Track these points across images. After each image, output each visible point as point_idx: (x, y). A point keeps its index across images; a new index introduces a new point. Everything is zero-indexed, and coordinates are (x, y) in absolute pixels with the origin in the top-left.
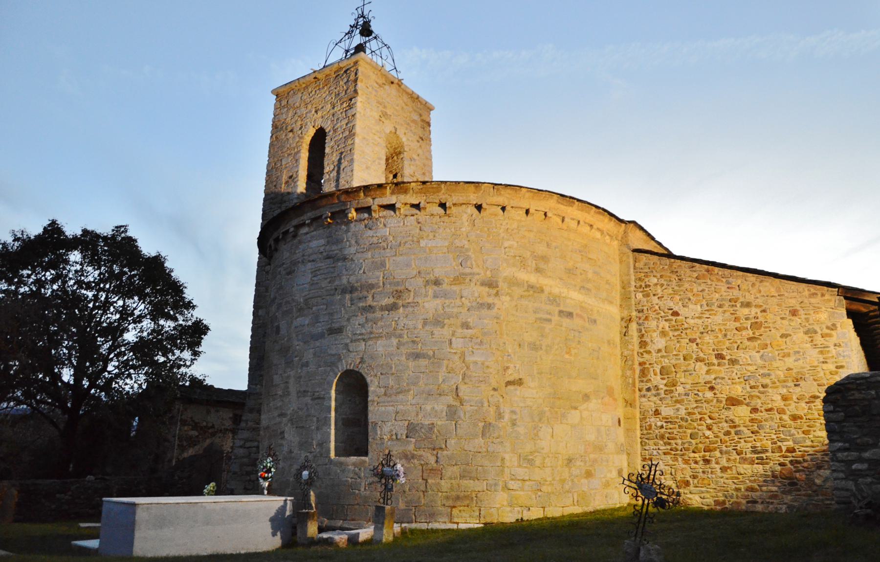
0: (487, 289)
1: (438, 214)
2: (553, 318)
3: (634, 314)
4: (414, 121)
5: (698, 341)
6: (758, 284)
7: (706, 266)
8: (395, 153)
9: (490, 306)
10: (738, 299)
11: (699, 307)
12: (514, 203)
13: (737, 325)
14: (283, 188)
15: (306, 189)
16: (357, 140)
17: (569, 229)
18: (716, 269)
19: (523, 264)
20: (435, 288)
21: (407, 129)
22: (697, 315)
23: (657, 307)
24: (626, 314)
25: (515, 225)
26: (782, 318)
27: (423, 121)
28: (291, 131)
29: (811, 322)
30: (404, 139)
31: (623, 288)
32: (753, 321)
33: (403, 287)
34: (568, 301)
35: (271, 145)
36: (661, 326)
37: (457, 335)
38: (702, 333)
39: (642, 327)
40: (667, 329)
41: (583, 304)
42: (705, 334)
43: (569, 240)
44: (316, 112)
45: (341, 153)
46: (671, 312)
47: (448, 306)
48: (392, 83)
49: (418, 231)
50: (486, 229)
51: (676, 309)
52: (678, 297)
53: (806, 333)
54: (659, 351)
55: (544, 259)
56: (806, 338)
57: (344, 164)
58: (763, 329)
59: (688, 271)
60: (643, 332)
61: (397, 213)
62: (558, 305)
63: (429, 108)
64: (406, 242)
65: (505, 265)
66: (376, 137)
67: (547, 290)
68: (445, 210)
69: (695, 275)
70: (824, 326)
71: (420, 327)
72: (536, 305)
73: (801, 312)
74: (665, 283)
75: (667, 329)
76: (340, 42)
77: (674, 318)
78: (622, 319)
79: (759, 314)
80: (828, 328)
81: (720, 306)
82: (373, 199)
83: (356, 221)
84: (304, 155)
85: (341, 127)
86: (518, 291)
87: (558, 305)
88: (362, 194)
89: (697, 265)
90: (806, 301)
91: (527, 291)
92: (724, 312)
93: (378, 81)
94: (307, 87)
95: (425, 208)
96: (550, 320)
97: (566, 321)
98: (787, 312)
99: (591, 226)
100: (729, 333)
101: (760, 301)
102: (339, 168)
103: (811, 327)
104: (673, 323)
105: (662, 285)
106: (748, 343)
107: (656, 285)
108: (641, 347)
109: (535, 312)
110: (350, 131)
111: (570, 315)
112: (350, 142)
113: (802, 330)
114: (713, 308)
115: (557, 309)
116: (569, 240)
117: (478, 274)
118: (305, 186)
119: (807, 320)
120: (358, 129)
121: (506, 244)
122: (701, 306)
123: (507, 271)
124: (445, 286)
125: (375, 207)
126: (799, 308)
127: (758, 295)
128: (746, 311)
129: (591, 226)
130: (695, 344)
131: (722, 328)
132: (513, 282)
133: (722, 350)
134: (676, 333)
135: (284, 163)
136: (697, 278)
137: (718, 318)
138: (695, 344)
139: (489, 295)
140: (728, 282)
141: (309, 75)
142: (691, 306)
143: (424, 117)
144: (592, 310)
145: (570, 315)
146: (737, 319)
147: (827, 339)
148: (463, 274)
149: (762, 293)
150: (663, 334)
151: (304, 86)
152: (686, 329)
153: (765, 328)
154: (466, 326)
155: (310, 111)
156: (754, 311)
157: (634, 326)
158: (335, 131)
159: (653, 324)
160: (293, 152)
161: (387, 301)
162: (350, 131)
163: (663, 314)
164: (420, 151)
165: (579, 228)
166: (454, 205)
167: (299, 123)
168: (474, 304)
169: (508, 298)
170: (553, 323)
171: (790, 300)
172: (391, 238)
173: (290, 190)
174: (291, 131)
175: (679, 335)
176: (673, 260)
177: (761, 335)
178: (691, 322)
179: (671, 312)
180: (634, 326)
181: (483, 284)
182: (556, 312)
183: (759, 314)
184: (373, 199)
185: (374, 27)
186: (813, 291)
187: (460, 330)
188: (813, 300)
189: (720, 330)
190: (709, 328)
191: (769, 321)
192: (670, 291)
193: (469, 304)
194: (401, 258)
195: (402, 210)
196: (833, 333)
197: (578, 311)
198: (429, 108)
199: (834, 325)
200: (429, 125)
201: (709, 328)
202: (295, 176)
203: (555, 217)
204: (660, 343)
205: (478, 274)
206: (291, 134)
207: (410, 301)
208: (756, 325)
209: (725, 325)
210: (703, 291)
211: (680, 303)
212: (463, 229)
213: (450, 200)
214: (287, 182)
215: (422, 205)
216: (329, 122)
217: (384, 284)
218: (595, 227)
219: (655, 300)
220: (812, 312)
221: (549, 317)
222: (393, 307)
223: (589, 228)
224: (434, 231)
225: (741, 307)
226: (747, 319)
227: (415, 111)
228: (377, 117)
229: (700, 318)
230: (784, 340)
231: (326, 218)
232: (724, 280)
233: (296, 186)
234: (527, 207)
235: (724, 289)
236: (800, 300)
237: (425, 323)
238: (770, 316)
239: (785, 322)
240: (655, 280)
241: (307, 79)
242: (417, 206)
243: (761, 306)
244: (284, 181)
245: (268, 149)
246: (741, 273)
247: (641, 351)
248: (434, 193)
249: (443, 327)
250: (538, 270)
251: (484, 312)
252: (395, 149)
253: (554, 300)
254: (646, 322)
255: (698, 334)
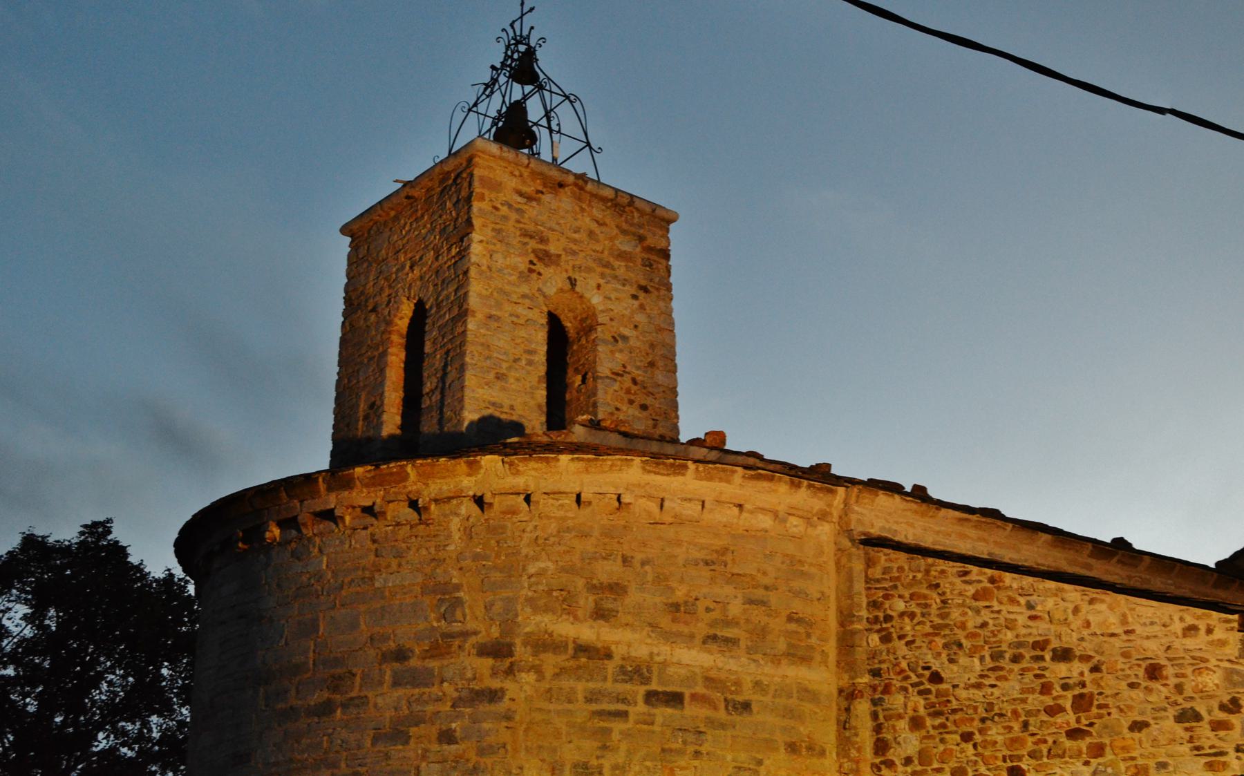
0: (490, 661)
1: (408, 523)
2: (631, 709)
3: (865, 679)
4: (622, 255)
5: (978, 738)
6: (1085, 607)
7: (989, 572)
8: (584, 329)
9: (494, 696)
10: (1047, 642)
11: (976, 661)
12: (549, 484)
13: (1048, 700)
14: (361, 428)
15: (402, 427)
16: (471, 325)
17: (679, 521)
18: (1008, 577)
19: (567, 605)
20: (396, 665)
21: (603, 275)
22: (973, 681)
23: (904, 665)
24: (845, 681)
25: (553, 527)
26: (1132, 686)
27: (649, 249)
28: (374, 310)
29: (1188, 692)
30: (596, 300)
31: (842, 624)
32: (1077, 691)
33: (345, 670)
34: (671, 670)
35: (343, 342)
36: (911, 705)
37: (432, 757)
38: (983, 720)
39: (879, 709)
40: (922, 711)
41: (713, 674)
42: (989, 723)
43: (679, 543)
44: (411, 267)
45: (447, 353)
46: (927, 673)
47: (418, 700)
48: (561, 185)
49: (372, 557)
50: (493, 543)
51: (936, 666)
52: (940, 641)
53: (1180, 718)
54: (908, 761)
55: (617, 589)
56: (1179, 729)
57: (452, 374)
58: (1094, 710)
59: (958, 581)
60: (881, 719)
61: (341, 525)
62: (646, 681)
63: (661, 219)
64: (353, 580)
65: (528, 610)
66: (520, 310)
67: (618, 651)
68: (419, 514)
69: (971, 590)
70: (1216, 706)
71: (368, 743)
72: (591, 685)
73: (1169, 671)
74: (918, 611)
75: (922, 711)
76: (476, 105)
77: (933, 688)
78: (841, 691)
79: (1088, 677)
80: (1223, 707)
81: (1016, 659)
82: (301, 502)
83: (279, 544)
84: (396, 358)
85: (448, 297)
86: (551, 661)
87: (646, 681)
88: (284, 495)
89: (975, 569)
90: (1177, 644)
91: (575, 657)
92: (1023, 671)
93: (525, 189)
94: (396, 218)
95: (383, 514)
96: (623, 715)
97: (663, 713)
98: (1141, 672)
99: (740, 506)
100: (1032, 720)
101: (1088, 647)
102: (444, 383)
103: (1188, 705)
104: (932, 698)
105: (912, 616)
106: (1068, 743)
107: (902, 615)
108: (876, 753)
109: (589, 700)
110: (460, 307)
111: (675, 699)
112: (459, 329)
113: (1172, 712)
114: (1002, 663)
115: (642, 690)
116: (679, 543)
117: (475, 633)
118: (398, 420)
119: (1179, 688)
120: (473, 301)
121: (532, 569)
122: (982, 659)
123: (532, 622)
124: (414, 662)
125: (304, 517)
126: (1163, 662)
127: (1085, 632)
128: (1062, 669)
129: (740, 506)
130: (970, 746)
131: (1019, 708)
132: (544, 644)
133: (1020, 758)
134: (937, 722)
135: (362, 377)
136: (975, 597)
137: (1012, 687)
138: (970, 746)
139: (494, 674)
140: (1030, 606)
141: (397, 192)
142: (963, 660)
143: (651, 241)
144: (737, 683)
145: (675, 699)
146: (1046, 689)
147: (1222, 733)
148: (452, 636)
149: (1094, 628)
150: (916, 723)
151: (393, 213)
152: (954, 711)
153: (1100, 707)
154: (447, 737)
155: (403, 267)
156: (1075, 670)
157: (862, 707)
158: (439, 306)
159: (896, 701)
160: (376, 354)
161: (317, 697)
162: (460, 307)
163: (914, 679)
164: (640, 318)
165: (707, 516)
166: (436, 501)
167: (387, 292)
168: (464, 693)
169: (531, 677)
170: (632, 718)
171: (1147, 644)
172: (330, 575)
173: (371, 433)
174: (374, 310)
175: (943, 726)
176: (930, 560)
177: (1091, 725)
178: (963, 694)
179: (927, 673)
180: (862, 707)
181: (483, 651)
182: (640, 698)
183: (1088, 677)
184: (301, 502)
185: (546, 63)
186: (1190, 620)
187: (435, 747)
188: (1190, 643)
189: (1015, 712)
190: (996, 710)
191: (1108, 692)
192: (928, 629)
193: (456, 695)
194: (343, 611)
195: (348, 519)
196: (1234, 719)
197: (700, 689)
198: (661, 219)
199: (1234, 701)
200: (666, 254)
201: (996, 710)
202: (378, 403)
203: (643, 502)
204: (909, 743)
205: (475, 633)
206: (373, 317)
207: (353, 694)
208: (1082, 703)
209: (1024, 701)
210: (984, 625)
211: (944, 656)
212: (451, 548)
213: (425, 493)
214: (366, 417)
215: (377, 508)
216: (431, 288)
217: (314, 664)
218: (747, 506)
219: (900, 647)
220: (1189, 671)
221: (621, 707)
222: (326, 709)
223: (736, 510)
224: (399, 555)
225: (1053, 659)
226: (1065, 687)
227: (624, 232)
228: (523, 266)
229: (978, 686)
230: (1137, 735)
231: (237, 542)
232: (1022, 600)
233: (379, 425)
234: (577, 490)
235: (1022, 620)
236: (1164, 641)
237: (375, 740)
238: (1110, 683)
239: (1138, 694)
240: (900, 605)
241: (395, 200)
242: (369, 510)
243: (1089, 658)
244: (361, 414)
245: (337, 349)
246: (1052, 585)
247: (877, 761)
248: (397, 482)
249: (407, 742)
250: (600, 614)
251: (485, 708)
252: (583, 321)
253: (636, 672)
254: (886, 697)
255: (977, 723)
